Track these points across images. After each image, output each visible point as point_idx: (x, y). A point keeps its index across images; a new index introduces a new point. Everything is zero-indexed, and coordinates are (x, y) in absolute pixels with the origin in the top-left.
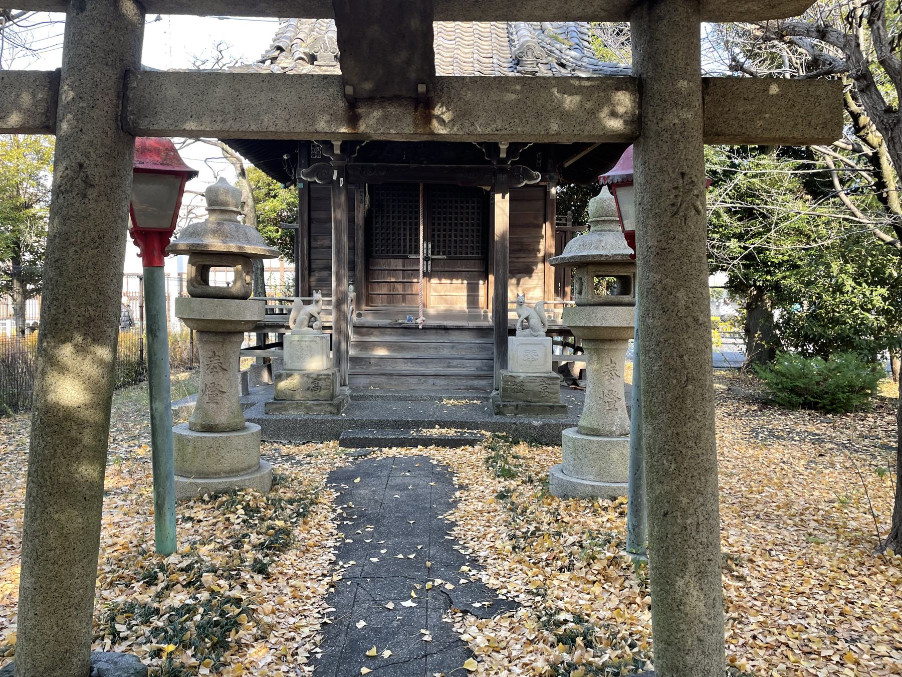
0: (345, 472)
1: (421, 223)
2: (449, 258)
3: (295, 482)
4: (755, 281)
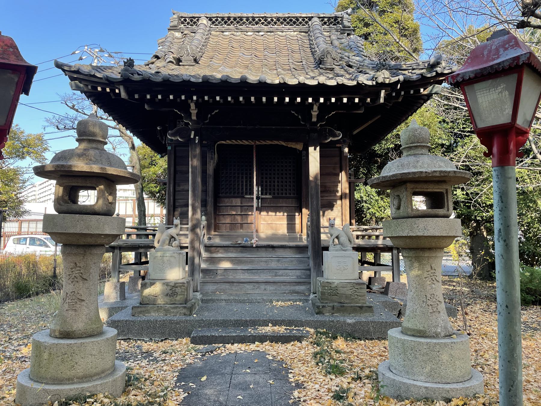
0: (194, 369)
1: (255, 173)
2: (274, 198)
3: (148, 383)
4: (475, 217)
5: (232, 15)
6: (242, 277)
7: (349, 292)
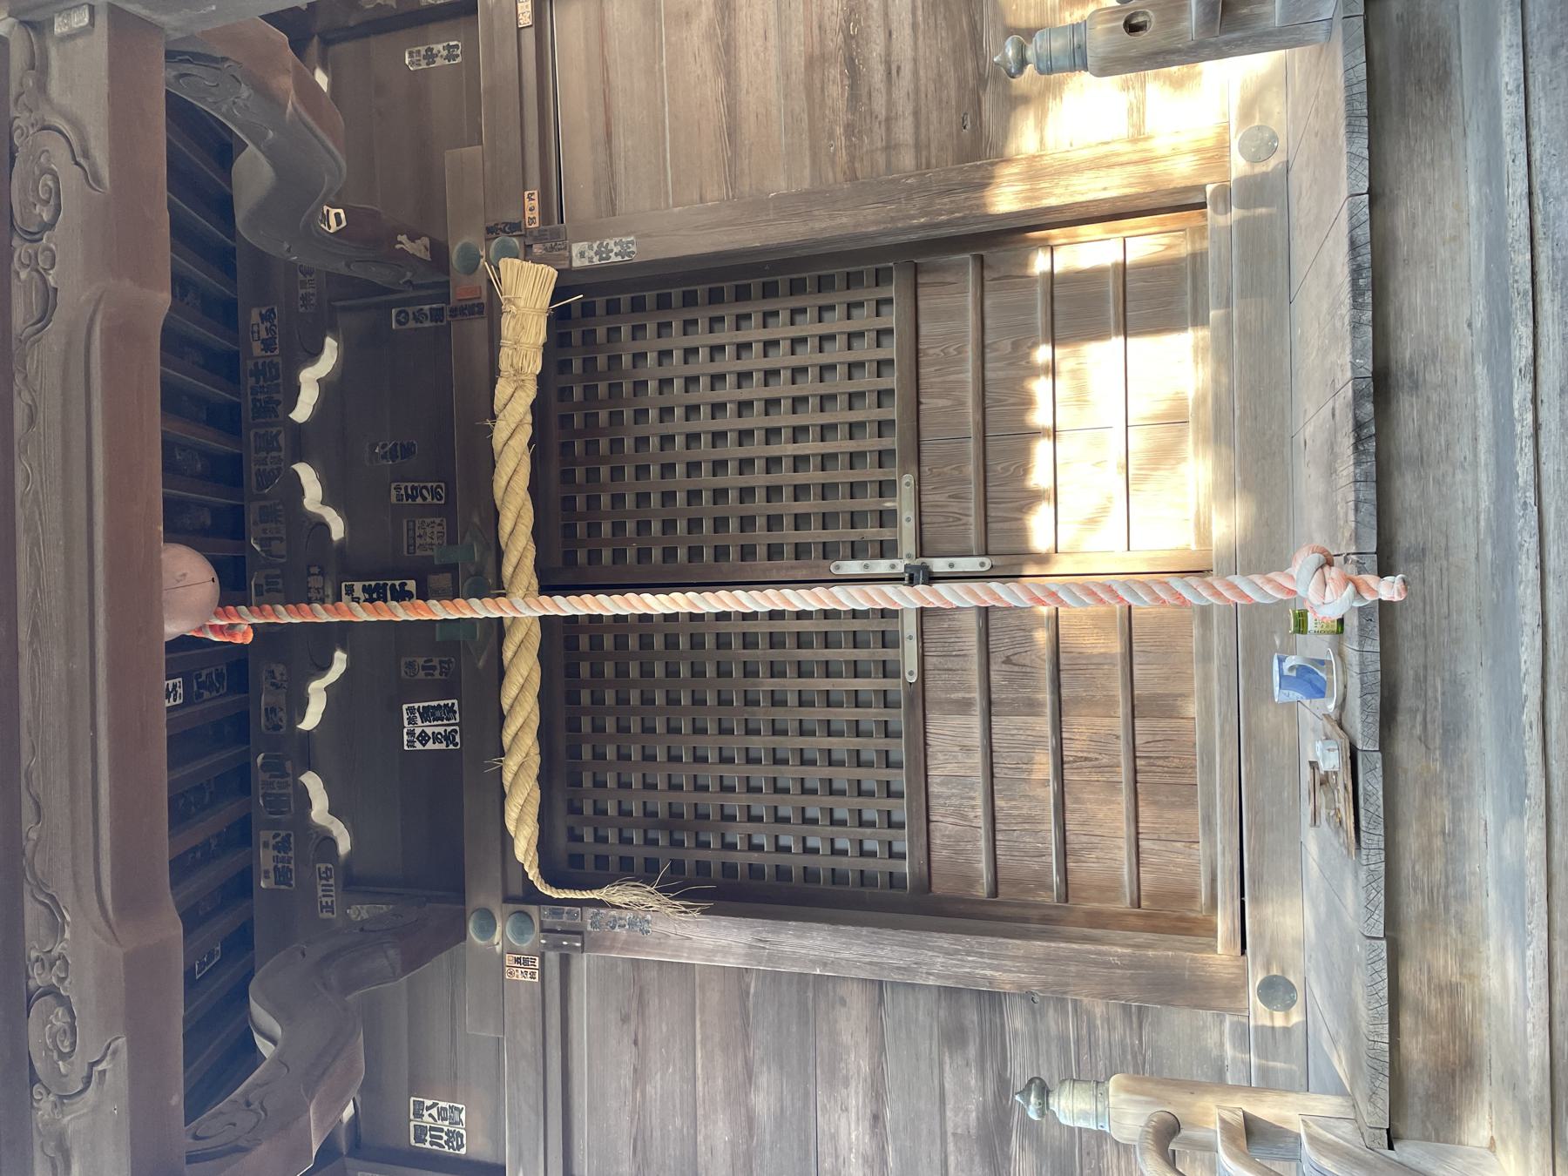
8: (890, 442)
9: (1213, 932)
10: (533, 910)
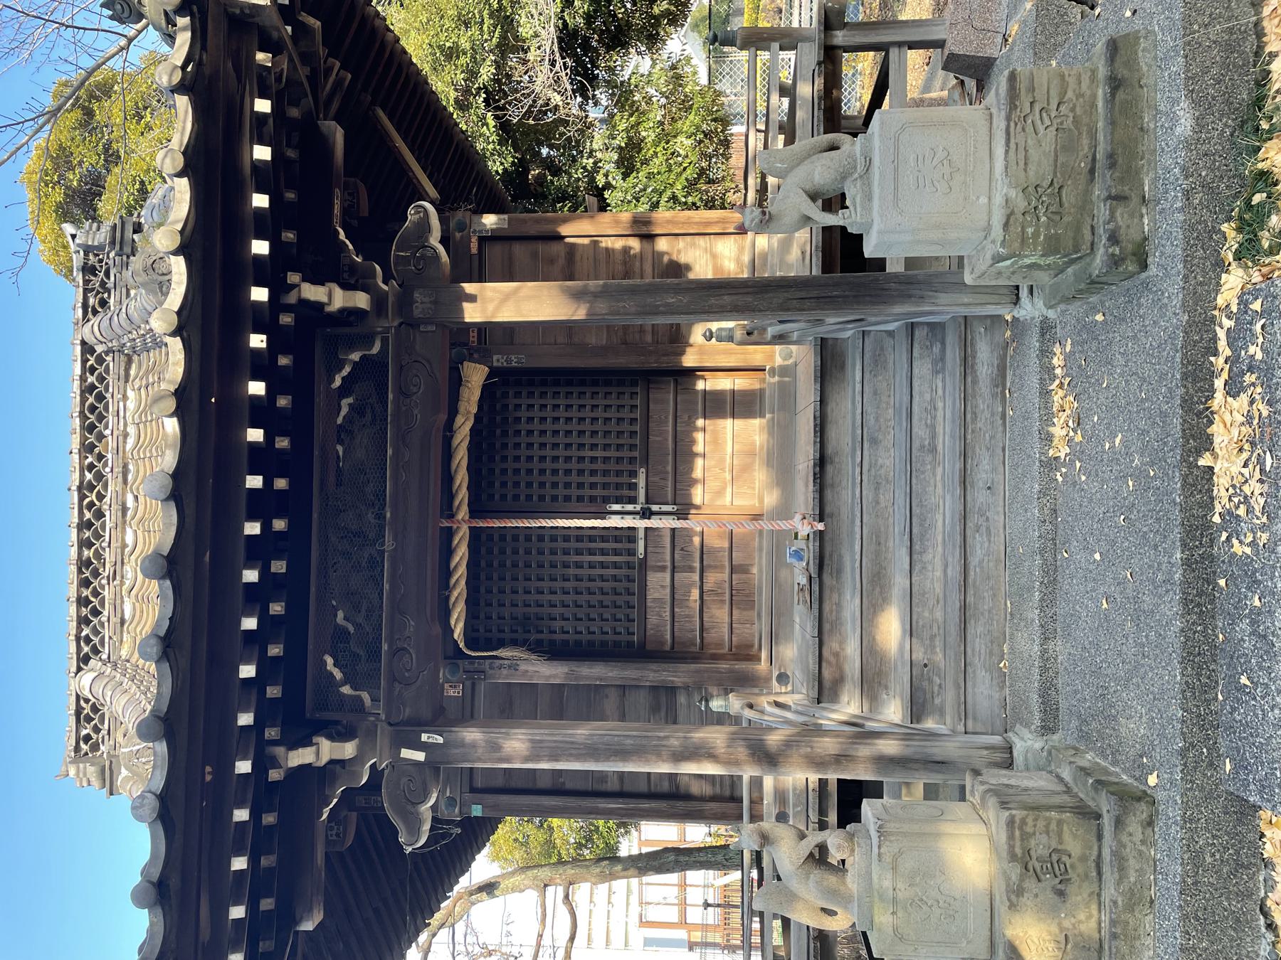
2: (646, 461)
5: (73, 592)
6: (938, 573)
7: (1049, 138)
8: (636, 454)
9: (760, 660)
10: (460, 662)
